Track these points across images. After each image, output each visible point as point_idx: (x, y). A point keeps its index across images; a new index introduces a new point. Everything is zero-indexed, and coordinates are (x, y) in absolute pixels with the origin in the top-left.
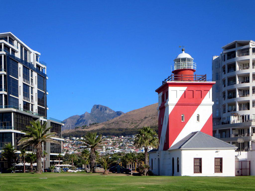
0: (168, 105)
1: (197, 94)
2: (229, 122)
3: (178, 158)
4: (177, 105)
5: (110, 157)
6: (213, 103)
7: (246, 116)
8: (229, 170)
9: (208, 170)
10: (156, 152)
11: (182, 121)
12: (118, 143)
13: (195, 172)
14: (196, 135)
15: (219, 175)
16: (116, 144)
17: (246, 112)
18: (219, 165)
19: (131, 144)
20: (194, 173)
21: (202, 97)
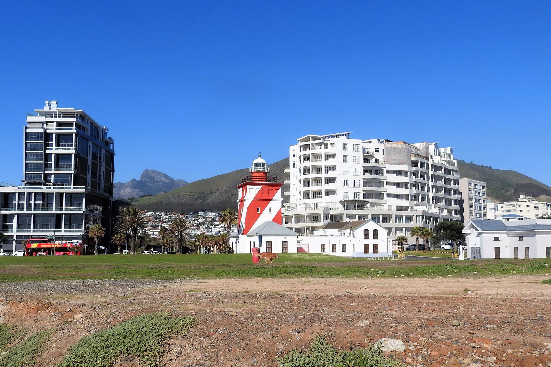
6: (282, 199)
18: (285, 245)
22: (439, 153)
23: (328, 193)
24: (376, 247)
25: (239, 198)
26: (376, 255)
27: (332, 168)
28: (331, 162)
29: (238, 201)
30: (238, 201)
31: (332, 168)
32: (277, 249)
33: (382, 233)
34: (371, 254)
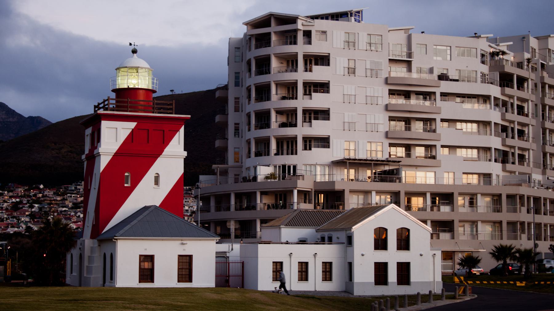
0: (99, 155)
2: (255, 178)
3: (112, 254)
5: (80, 197)
6: (185, 154)
7: (289, 167)
8: (204, 277)
9: (166, 277)
11: (126, 185)
12: (26, 204)
13: (141, 281)
14: (147, 212)
16: (22, 208)
17: (288, 160)
18: (185, 267)
19: (63, 207)
20: (179, 281)
21: (165, 142)
22: (545, 166)
23: (310, 142)
24: (404, 269)
25: (87, 152)
26: (403, 290)
27: (323, 87)
28: (319, 73)
29: (83, 157)
30: (83, 157)
31: (323, 87)
32: (166, 277)
33: (421, 234)
34: (393, 287)
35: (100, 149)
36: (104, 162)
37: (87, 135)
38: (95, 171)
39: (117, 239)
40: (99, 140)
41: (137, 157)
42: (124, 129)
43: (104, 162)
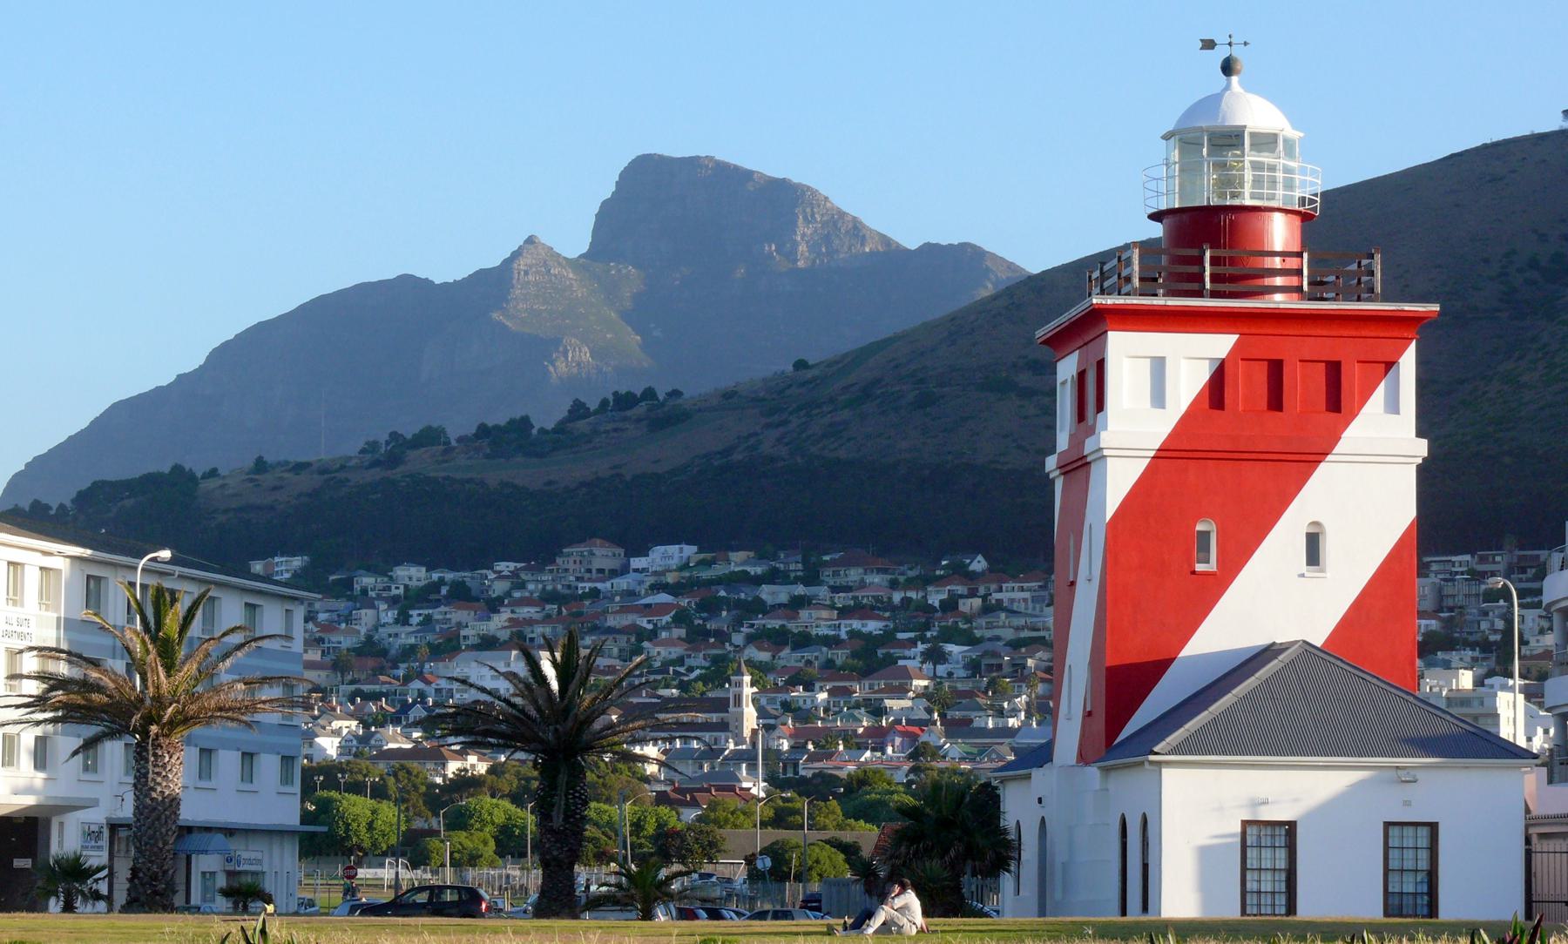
1: (1304, 384)
4: (1165, 454)
6: (1421, 448)
10: (1028, 777)
11: (1200, 567)
12: (912, 643)
15: (1144, 918)
21: (1338, 402)
25: (1063, 442)
29: (1051, 463)
35: (1103, 435)
36: (1117, 481)
37: (1064, 383)
38: (1090, 517)
39: (1159, 763)
40: (1100, 406)
41: (1244, 457)
42: (1193, 358)
43: (1117, 481)
